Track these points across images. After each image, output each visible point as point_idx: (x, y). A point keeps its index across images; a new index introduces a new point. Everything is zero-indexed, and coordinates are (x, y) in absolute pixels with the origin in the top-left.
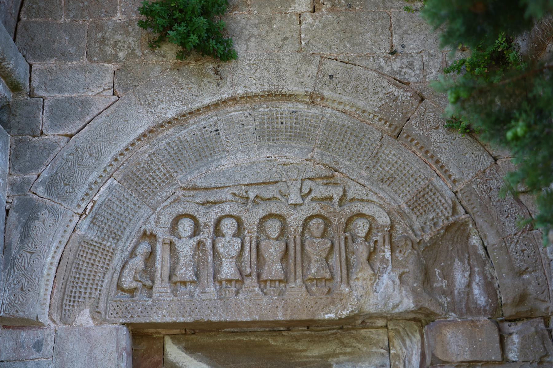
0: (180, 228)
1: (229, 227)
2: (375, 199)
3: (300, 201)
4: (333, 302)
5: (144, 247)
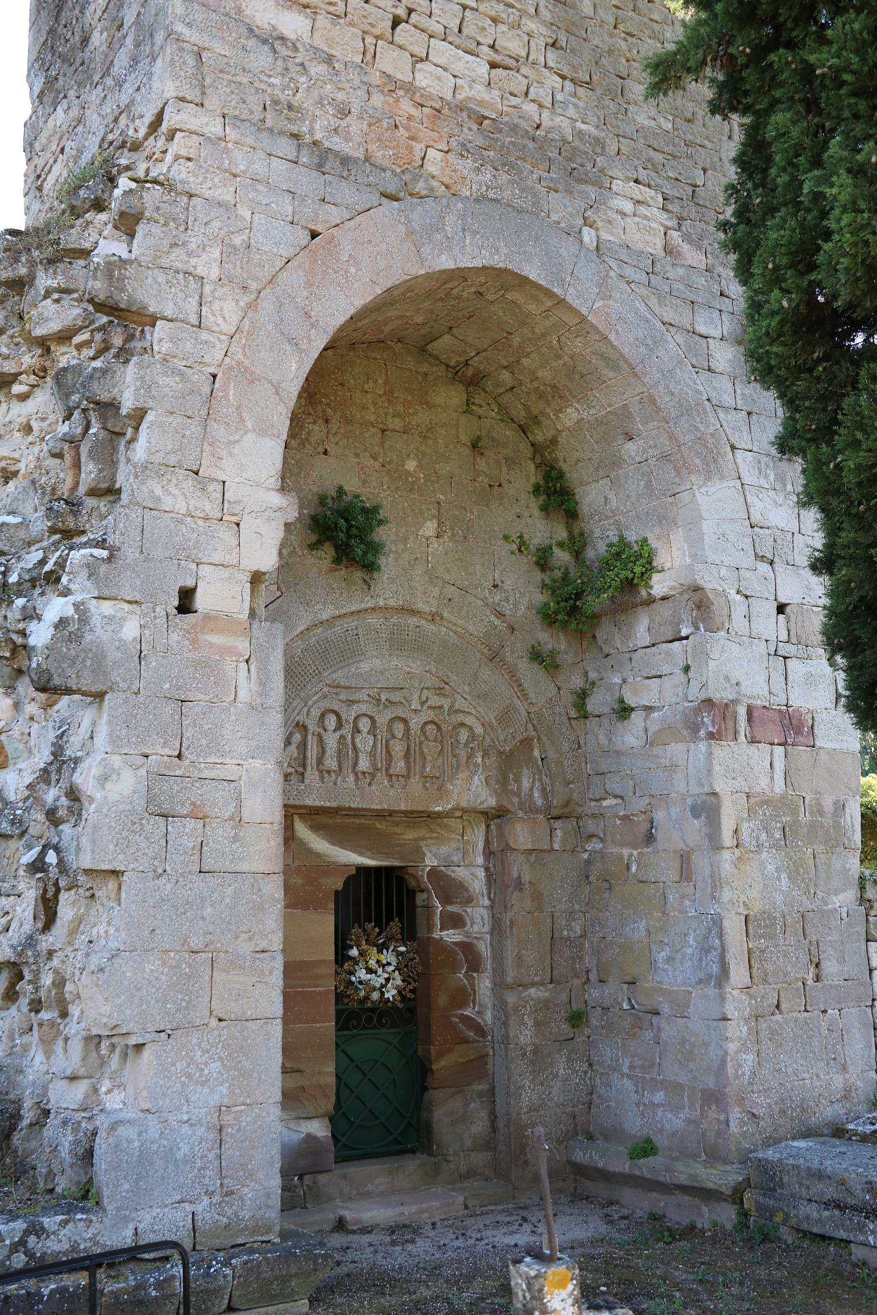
0: (327, 722)
1: (364, 725)
2: (473, 712)
3: (419, 708)
4: (441, 798)
5: (297, 737)
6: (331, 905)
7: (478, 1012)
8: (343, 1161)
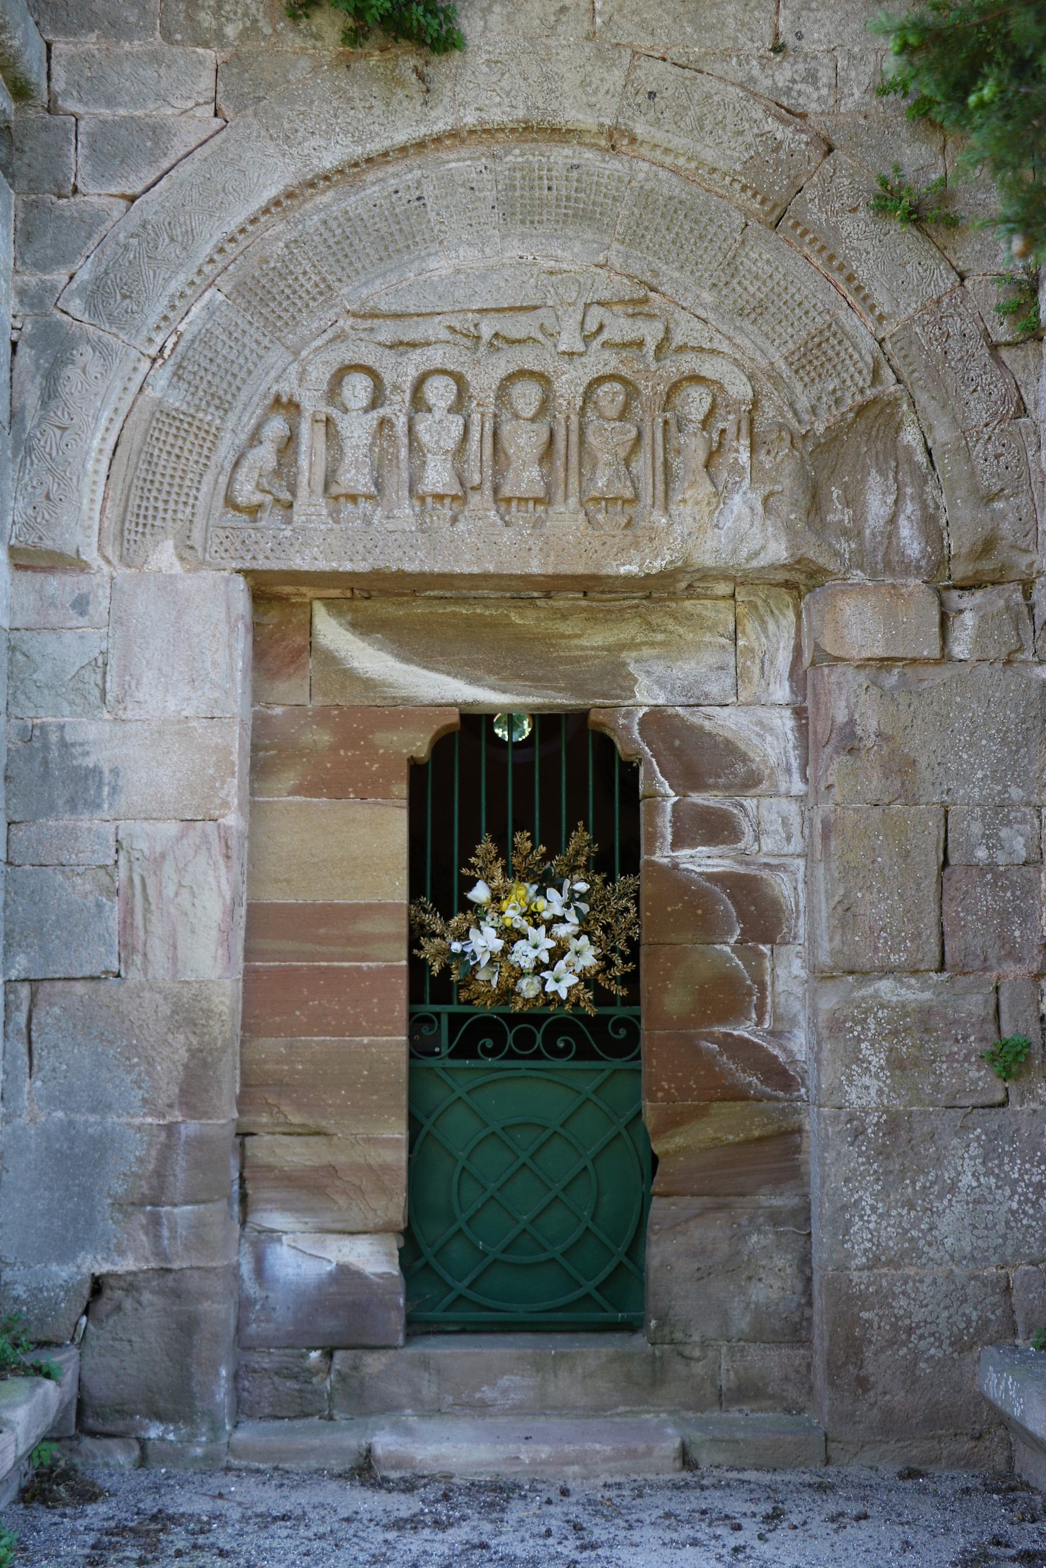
0: (347, 392)
2: (725, 347)
3: (580, 347)
4: (636, 544)
5: (277, 427)
6: (401, 789)
7: (772, 1033)
8: (463, 1331)
